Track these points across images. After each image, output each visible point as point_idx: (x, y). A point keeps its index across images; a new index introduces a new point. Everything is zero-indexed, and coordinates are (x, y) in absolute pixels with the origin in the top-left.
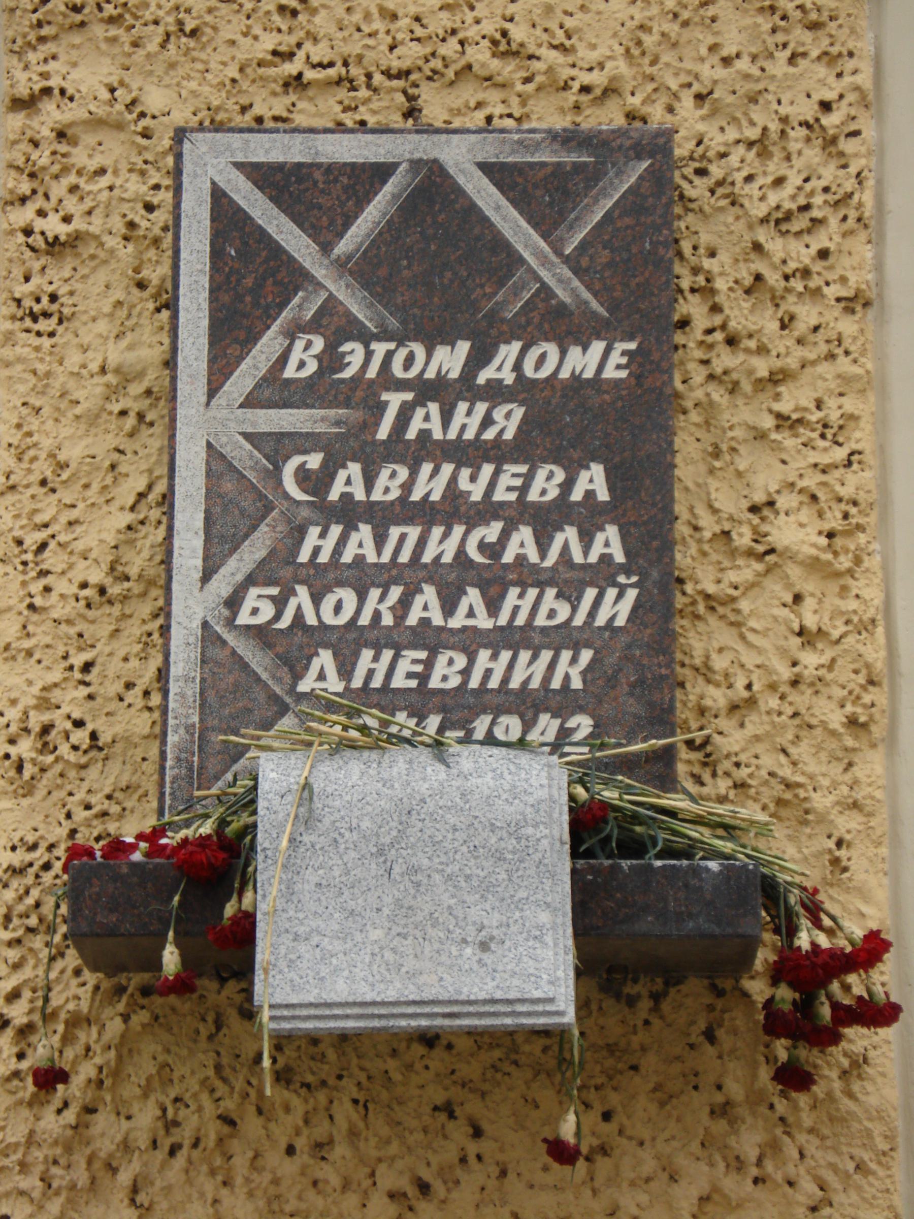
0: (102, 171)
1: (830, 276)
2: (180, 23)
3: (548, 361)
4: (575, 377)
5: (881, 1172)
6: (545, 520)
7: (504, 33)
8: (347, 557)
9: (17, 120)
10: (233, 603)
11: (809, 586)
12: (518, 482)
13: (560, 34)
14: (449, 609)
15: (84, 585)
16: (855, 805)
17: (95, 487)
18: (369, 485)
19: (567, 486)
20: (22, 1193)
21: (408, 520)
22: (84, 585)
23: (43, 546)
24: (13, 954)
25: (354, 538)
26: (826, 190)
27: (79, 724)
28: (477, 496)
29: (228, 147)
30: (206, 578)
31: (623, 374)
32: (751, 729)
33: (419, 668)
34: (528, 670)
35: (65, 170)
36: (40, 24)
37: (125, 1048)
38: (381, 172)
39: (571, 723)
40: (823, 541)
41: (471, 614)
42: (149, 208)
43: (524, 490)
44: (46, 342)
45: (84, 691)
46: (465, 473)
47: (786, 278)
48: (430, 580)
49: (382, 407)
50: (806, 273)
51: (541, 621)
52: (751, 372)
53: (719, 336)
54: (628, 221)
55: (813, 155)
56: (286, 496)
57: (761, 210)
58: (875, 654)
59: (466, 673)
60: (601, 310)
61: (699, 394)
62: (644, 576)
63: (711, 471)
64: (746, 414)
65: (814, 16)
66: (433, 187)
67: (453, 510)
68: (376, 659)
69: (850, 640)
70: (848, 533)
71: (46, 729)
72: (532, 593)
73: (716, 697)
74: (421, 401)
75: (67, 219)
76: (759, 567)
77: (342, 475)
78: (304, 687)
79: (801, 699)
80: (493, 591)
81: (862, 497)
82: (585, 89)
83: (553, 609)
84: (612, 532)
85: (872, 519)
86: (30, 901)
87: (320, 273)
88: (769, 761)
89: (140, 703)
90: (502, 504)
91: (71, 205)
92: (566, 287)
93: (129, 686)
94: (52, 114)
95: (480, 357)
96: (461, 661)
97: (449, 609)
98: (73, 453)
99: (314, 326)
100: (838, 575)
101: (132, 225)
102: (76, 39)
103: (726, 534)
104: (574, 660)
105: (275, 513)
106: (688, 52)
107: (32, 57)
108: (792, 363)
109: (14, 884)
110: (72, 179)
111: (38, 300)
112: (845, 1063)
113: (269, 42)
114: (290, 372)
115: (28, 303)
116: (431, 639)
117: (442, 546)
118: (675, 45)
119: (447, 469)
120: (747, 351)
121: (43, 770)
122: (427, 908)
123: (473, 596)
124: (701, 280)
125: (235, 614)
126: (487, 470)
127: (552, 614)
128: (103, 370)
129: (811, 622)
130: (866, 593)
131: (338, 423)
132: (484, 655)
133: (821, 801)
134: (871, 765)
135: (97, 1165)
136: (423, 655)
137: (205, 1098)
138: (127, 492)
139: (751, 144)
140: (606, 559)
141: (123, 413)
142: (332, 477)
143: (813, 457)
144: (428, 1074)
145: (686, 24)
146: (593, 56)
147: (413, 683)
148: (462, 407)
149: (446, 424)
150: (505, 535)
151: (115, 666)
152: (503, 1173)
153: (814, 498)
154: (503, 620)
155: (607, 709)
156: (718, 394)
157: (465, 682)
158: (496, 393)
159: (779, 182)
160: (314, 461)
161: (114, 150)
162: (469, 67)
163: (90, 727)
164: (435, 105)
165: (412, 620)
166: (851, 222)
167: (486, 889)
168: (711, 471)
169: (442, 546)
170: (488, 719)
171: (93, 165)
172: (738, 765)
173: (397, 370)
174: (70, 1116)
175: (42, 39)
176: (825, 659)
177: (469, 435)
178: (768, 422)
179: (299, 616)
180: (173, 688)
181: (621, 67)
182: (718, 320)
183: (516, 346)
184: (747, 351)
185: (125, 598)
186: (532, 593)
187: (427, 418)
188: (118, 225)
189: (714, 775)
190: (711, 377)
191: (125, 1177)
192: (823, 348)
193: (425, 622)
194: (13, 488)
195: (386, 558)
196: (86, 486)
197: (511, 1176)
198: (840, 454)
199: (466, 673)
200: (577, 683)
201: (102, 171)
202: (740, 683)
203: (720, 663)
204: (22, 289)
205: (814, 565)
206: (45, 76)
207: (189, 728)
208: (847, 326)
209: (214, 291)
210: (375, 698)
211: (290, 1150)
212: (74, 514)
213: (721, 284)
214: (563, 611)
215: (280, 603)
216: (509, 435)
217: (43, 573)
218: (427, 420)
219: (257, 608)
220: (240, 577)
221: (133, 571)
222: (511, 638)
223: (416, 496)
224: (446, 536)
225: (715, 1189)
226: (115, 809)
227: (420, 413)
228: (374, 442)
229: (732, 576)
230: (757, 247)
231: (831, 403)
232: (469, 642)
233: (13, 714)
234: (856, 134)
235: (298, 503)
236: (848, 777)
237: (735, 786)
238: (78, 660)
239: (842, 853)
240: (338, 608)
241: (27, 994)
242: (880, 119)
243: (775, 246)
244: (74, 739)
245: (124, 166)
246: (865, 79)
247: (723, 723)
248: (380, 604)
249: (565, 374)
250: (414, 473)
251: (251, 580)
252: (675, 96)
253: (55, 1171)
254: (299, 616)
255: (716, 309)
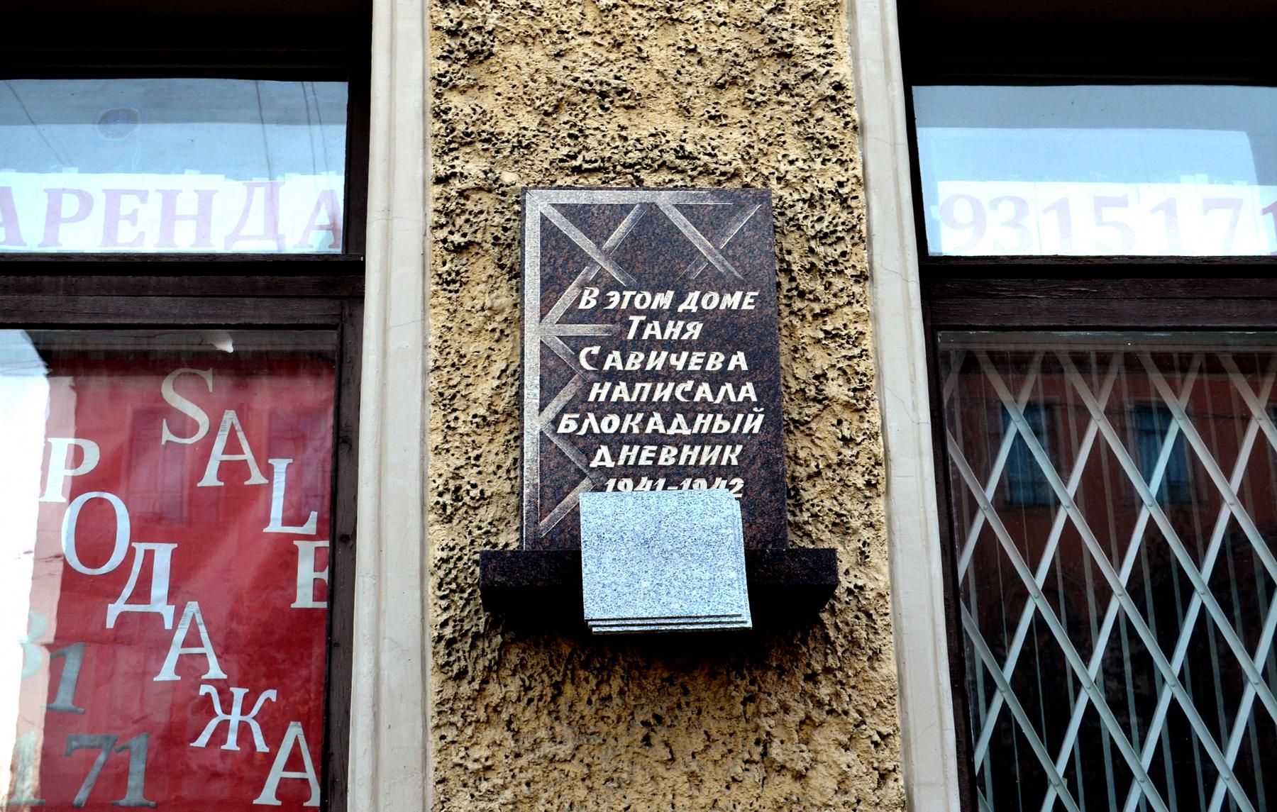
0: (481, 212)
1: (847, 265)
2: (519, 142)
3: (712, 301)
4: (728, 309)
5: (890, 707)
6: (716, 380)
7: (682, 147)
8: (614, 399)
9: (438, 189)
10: (556, 422)
11: (846, 415)
12: (701, 361)
13: (709, 149)
14: (668, 425)
15: (475, 416)
16: (872, 525)
17: (480, 367)
18: (624, 363)
19: (726, 363)
20: (452, 724)
21: (645, 381)
22: (475, 416)
23: (454, 397)
24: (444, 603)
25: (617, 389)
26: (843, 223)
27: (474, 486)
28: (680, 368)
29: (549, 197)
30: (541, 409)
31: (752, 307)
32: (819, 488)
33: (653, 455)
34: (710, 456)
35: (463, 212)
36: (450, 142)
37: (504, 647)
38: (626, 208)
39: (732, 482)
40: (851, 394)
41: (679, 427)
42: (505, 229)
43: (705, 364)
44: (454, 295)
45: (476, 470)
46: (674, 356)
47: (826, 265)
48: (657, 410)
49: (630, 323)
50: (835, 263)
51: (715, 430)
52: (812, 310)
53: (795, 293)
54: (751, 233)
55: (835, 207)
56: (582, 367)
57: (812, 233)
58: (880, 451)
59: (678, 457)
60: (739, 276)
61: (786, 320)
62: (767, 407)
63: (794, 359)
64: (808, 331)
65: (833, 142)
66: (651, 214)
67: (668, 374)
68: (630, 450)
69: (866, 442)
70: (863, 390)
71: (458, 488)
72: (710, 417)
73: (802, 472)
74: (650, 320)
75: (464, 235)
76: (820, 407)
77: (610, 357)
78: (594, 464)
79: (843, 472)
80: (690, 415)
81: (868, 372)
82: (723, 174)
83: (721, 425)
84: (750, 386)
85: (874, 383)
86: (452, 576)
87: (596, 257)
88: (827, 503)
89: (504, 476)
90: (694, 372)
91: (466, 229)
92: (720, 264)
93: (499, 467)
94: (457, 184)
95: (679, 299)
96: (675, 451)
97: (668, 425)
98: (468, 350)
99: (594, 283)
100: (858, 410)
101: (496, 238)
102: (468, 150)
103: (803, 390)
104: (733, 451)
105: (576, 377)
106: (773, 158)
107: (446, 158)
108: (832, 306)
109: (444, 566)
110: (467, 216)
111: (450, 275)
112: (870, 653)
113: (565, 150)
114: (582, 306)
115: (445, 276)
116: (658, 440)
117: (663, 393)
118: (765, 155)
119: (664, 354)
120: (809, 300)
121: (457, 510)
122: (672, 571)
123: (680, 418)
124: (785, 266)
125: (557, 428)
126: (685, 355)
127: (721, 427)
128: (483, 309)
129: (847, 433)
130: (872, 420)
131: (608, 331)
132: (686, 448)
133: (855, 523)
134: (879, 505)
135: (490, 710)
136: (655, 448)
137: (544, 676)
138: (496, 369)
139: (804, 201)
140: (747, 399)
141: (493, 330)
142: (605, 358)
143: (844, 353)
144: (673, 660)
145: (770, 144)
146: (727, 158)
147: (650, 463)
148: (671, 323)
149: (663, 331)
150: (695, 387)
151: (492, 457)
152: (699, 713)
153: (845, 373)
154: (695, 431)
155: (749, 475)
156: (796, 321)
157: (677, 462)
158: (688, 316)
159: (820, 219)
160: (596, 350)
161: (488, 201)
162: (664, 162)
163: (480, 488)
164: (650, 179)
165: (649, 430)
166: (856, 239)
167: (702, 561)
168: (794, 359)
169: (663, 393)
170: (689, 480)
171: (476, 210)
172: (813, 505)
173: (637, 304)
174: (476, 685)
175: (452, 150)
176: (854, 452)
177: (675, 337)
178: (822, 335)
179: (590, 428)
180: (526, 466)
181: (739, 164)
182: (794, 285)
183: (697, 293)
184: (809, 300)
185: (496, 423)
186: (710, 417)
187: (653, 329)
188: (489, 238)
189: (801, 511)
190: (792, 313)
191: (505, 716)
192: (846, 299)
193: (655, 431)
194: (438, 368)
195: (634, 399)
196: (475, 367)
197: (704, 714)
198: (857, 351)
199: (678, 457)
200: (735, 462)
201: (481, 212)
202: (813, 464)
203: (802, 454)
204: (441, 270)
205: (847, 405)
206: (453, 167)
207: (535, 485)
208: (857, 289)
209: (543, 265)
210: (630, 471)
211: (589, 702)
212: (470, 380)
213: (795, 267)
214: (727, 426)
215: (580, 422)
216: (695, 337)
217: (455, 410)
218: (653, 330)
219: (568, 424)
220: (558, 409)
221: (500, 409)
222: (699, 440)
223: (649, 368)
224: (664, 388)
225: (808, 717)
226: (494, 530)
227: (649, 326)
228: (626, 341)
229: (807, 411)
230: (811, 250)
231: (852, 326)
232: (678, 441)
233: (440, 481)
234: (856, 197)
235: (587, 371)
236: (867, 511)
237: (812, 516)
238: (473, 454)
239: (866, 549)
240: (610, 424)
241: (451, 623)
242: (866, 190)
243: (821, 250)
244: (472, 494)
245: (492, 210)
246: (859, 172)
247: (805, 485)
248: (632, 423)
249: (722, 307)
250: (647, 356)
251: (564, 411)
252: (767, 178)
253: (468, 713)
254: (590, 428)
255: (793, 279)
